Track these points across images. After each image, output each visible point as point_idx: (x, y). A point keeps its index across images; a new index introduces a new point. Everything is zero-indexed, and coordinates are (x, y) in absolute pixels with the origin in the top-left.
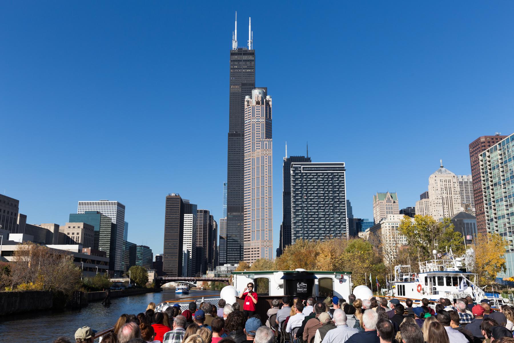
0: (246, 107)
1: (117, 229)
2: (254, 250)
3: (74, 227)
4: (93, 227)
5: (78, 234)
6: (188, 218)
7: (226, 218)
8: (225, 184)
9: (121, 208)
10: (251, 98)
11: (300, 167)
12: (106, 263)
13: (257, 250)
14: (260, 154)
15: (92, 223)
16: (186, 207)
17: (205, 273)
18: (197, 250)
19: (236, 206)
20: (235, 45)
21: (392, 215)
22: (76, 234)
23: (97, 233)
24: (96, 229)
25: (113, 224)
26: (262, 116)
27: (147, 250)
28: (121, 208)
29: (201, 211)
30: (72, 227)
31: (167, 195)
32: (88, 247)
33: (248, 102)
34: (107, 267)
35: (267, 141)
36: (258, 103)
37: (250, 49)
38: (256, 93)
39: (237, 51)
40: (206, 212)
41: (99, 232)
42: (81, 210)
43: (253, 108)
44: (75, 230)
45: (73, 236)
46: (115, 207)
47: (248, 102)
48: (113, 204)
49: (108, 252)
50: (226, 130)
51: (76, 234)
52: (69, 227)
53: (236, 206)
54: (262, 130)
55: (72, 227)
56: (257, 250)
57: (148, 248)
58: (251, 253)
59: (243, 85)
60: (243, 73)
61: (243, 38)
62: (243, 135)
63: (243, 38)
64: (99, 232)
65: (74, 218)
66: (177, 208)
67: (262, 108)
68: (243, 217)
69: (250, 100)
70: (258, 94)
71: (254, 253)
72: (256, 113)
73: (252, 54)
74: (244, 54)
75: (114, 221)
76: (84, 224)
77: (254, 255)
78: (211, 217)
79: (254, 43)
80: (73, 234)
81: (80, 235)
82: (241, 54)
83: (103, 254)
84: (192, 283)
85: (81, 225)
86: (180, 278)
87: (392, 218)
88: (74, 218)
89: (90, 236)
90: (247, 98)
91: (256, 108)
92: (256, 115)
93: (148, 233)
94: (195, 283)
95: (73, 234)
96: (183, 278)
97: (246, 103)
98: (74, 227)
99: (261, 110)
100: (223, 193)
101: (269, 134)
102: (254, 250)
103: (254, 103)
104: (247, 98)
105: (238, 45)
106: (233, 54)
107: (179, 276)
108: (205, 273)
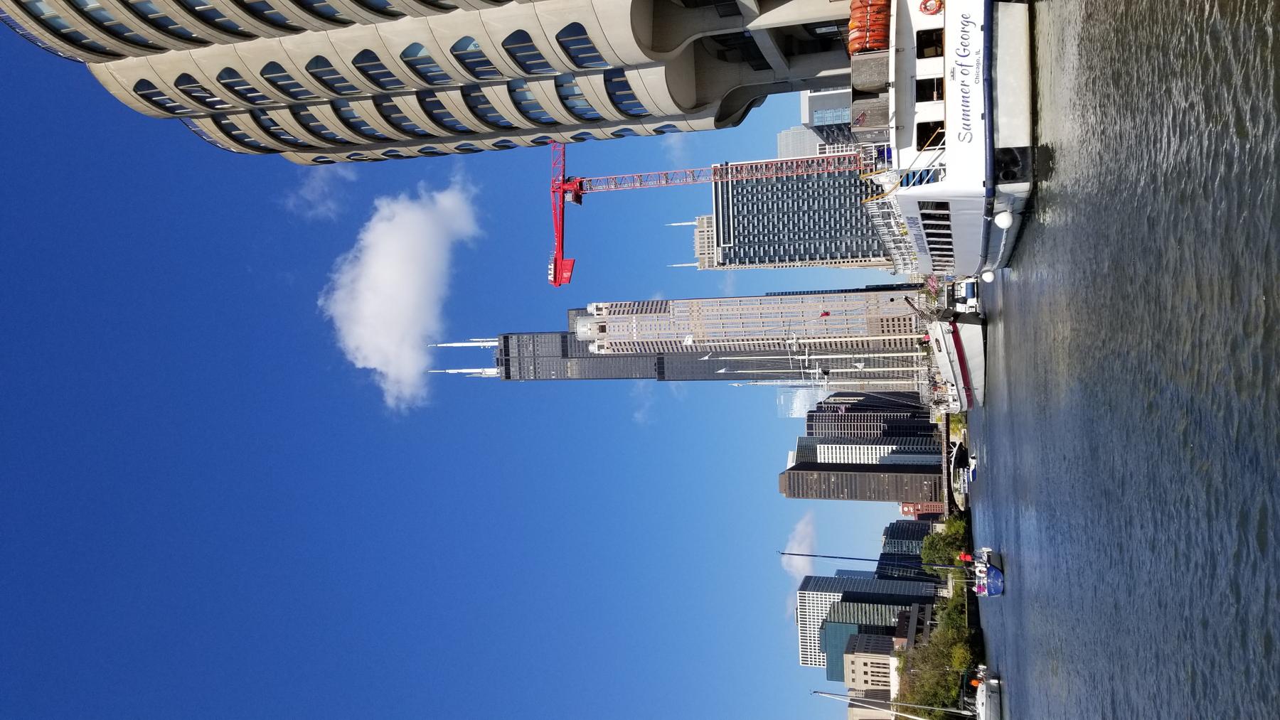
0: (609, 352)
1: (854, 592)
4: (852, 636)
5: (865, 664)
6: (825, 454)
9: (809, 584)
11: (724, 249)
12: (922, 610)
13: (885, 323)
15: (846, 640)
16: (807, 463)
17: (936, 426)
18: (889, 435)
20: (492, 372)
23: (865, 629)
24: (855, 630)
25: (844, 599)
27: (896, 532)
28: (809, 584)
30: (854, 676)
31: (729, 131)
32: (892, 643)
33: (600, 347)
34: (928, 607)
39: (503, 368)
41: (860, 627)
42: (819, 661)
46: (810, 595)
47: (600, 347)
48: (803, 599)
49: (898, 609)
55: (854, 676)
56: (885, 323)
59: (565, 354)
63: (480, 357)
64: (860, 627)
70: (585, 329)
73: (506, 339)
74: (507, 354)
75: (838, 597)
80: (866, 673)
82: (507, 361)
83: (904, 617)
84: (955, 450)
85: (848, 658)
86: (945, 472)
88: (835, 673)
89: (874, 639)
90: (593, 348)
93: (859, 531)
94: (954, 444)
95: (866, 673)
96: (944, 465)
97: (603, 352)
104: (593, 348)
106: (508, 376)
107: (941, 472)
108: (936, 426)
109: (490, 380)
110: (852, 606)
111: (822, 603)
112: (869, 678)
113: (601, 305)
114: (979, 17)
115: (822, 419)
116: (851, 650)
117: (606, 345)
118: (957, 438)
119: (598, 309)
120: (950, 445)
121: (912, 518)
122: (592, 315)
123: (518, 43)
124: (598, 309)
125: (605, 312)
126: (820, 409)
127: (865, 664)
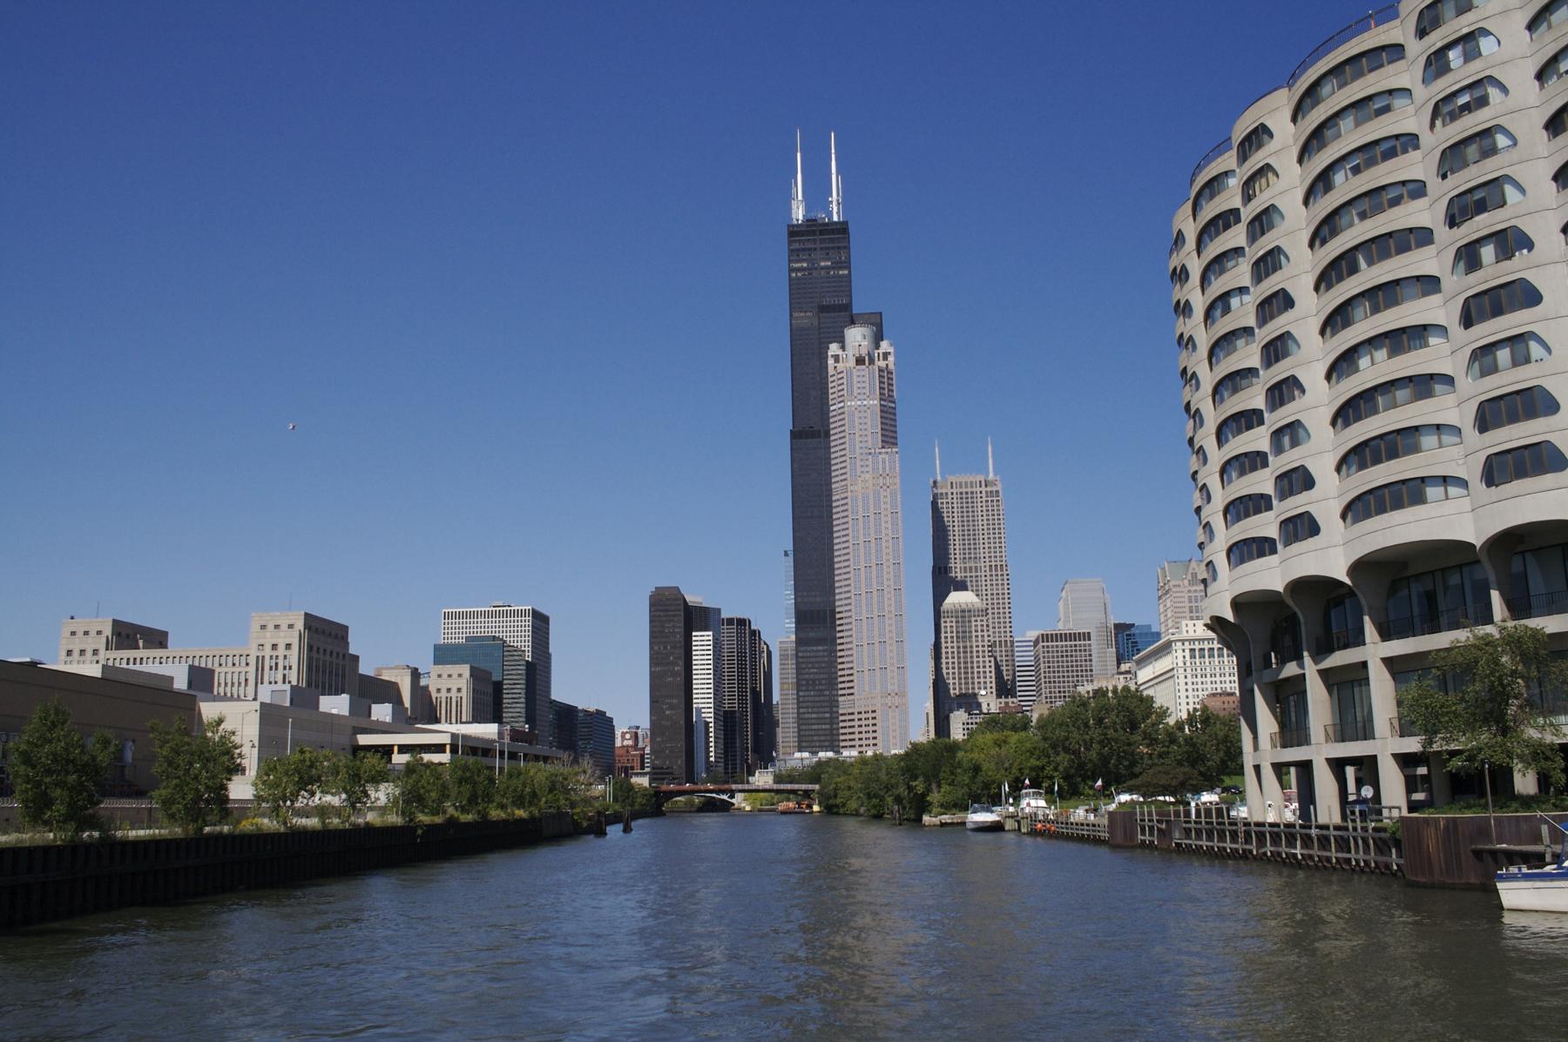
0: (831, 371)
2: (863, 716)
3: (86, 633)
5: (459, 690)
6: (702, 641)
7: (793, 637)
8: (786, 554)
9: (540, 622)
10: (843, 348)
13: (870, 715)
14: (870, 484)
15: (482, 666)
16: (697, 617)
18: (727, 720)
19: (817, 618)
21: (1191, 623)
22: (454, 690)
23: (498, 687)
24: (496, 677)
26: (872, 390)
27: (602, 722)
28: (540, 622)
29: (730, 621)
30: (445, 676)
33: (837, 358)
35: (889, 459)
36: (860, 361)
37: (835, 219)
38: (857, 336)
40: (742, 622)
42: (457, 635)
43: (850, 372)
44: (452, 683)
45: (274, 654)
47: (837, 358)
50: (784, 423)
51: (454, 690)
52: (73, 633)
53: (817, 618)
54: (873, 425)
55: (445, 676)
56: (870, 715)
57: (611, 720)
58: (856, 723)
59: (823, 309)
60: (821, 284)
61: (817, 192)
62: (828, 435)
63: (817, 192)
65: (444, 654)
66: (675, 620)
67: (871, 374)
68: (835, 639)
69: (840, 352)
70: (859, 338)
71: (864, 736)
72: (856, 385)
73: (842, 229)
76: (472, 669)
77: (864, 729)
78: (755, 634)
79: (845, 203)
80: (449, 690)
81: (464, 693)
82: (814, 233)
84: (725, 797)
85: (465, 670)
87: (1191, 629)
88: (444, 654)
90: (834, 348)
91: (855, 373)
92: (856, 392)
93: (606, 677)
94: (732, 797)
95: (274, 647)
97: (831, 362)
98: (86, 633)
99: (865, 378)
100: (784, 570)
101: (889, 437)
102: (863, 716)
103: (852, 362)
104: (834, 348)
105: (807, 209)
109: (789, 210)
110: (522, 669)
111: (520, 637)
112: (444, 694)
113: (891, 358)
114: (680, 638)
115: (740, 635)
116: (475, 673)
117: (840, 366)
118: (739, 800)
119: (886, 355)
120: (732, 794)
121: (618, 743)
122: (877, 347)
123: (1511, 242)
124: (886, 355)
125: (882, 364)
126: (754, 633)
127: (459, 690)
